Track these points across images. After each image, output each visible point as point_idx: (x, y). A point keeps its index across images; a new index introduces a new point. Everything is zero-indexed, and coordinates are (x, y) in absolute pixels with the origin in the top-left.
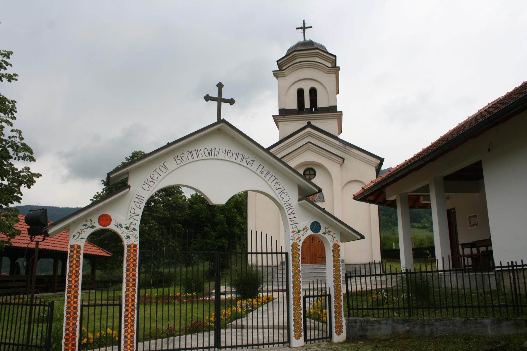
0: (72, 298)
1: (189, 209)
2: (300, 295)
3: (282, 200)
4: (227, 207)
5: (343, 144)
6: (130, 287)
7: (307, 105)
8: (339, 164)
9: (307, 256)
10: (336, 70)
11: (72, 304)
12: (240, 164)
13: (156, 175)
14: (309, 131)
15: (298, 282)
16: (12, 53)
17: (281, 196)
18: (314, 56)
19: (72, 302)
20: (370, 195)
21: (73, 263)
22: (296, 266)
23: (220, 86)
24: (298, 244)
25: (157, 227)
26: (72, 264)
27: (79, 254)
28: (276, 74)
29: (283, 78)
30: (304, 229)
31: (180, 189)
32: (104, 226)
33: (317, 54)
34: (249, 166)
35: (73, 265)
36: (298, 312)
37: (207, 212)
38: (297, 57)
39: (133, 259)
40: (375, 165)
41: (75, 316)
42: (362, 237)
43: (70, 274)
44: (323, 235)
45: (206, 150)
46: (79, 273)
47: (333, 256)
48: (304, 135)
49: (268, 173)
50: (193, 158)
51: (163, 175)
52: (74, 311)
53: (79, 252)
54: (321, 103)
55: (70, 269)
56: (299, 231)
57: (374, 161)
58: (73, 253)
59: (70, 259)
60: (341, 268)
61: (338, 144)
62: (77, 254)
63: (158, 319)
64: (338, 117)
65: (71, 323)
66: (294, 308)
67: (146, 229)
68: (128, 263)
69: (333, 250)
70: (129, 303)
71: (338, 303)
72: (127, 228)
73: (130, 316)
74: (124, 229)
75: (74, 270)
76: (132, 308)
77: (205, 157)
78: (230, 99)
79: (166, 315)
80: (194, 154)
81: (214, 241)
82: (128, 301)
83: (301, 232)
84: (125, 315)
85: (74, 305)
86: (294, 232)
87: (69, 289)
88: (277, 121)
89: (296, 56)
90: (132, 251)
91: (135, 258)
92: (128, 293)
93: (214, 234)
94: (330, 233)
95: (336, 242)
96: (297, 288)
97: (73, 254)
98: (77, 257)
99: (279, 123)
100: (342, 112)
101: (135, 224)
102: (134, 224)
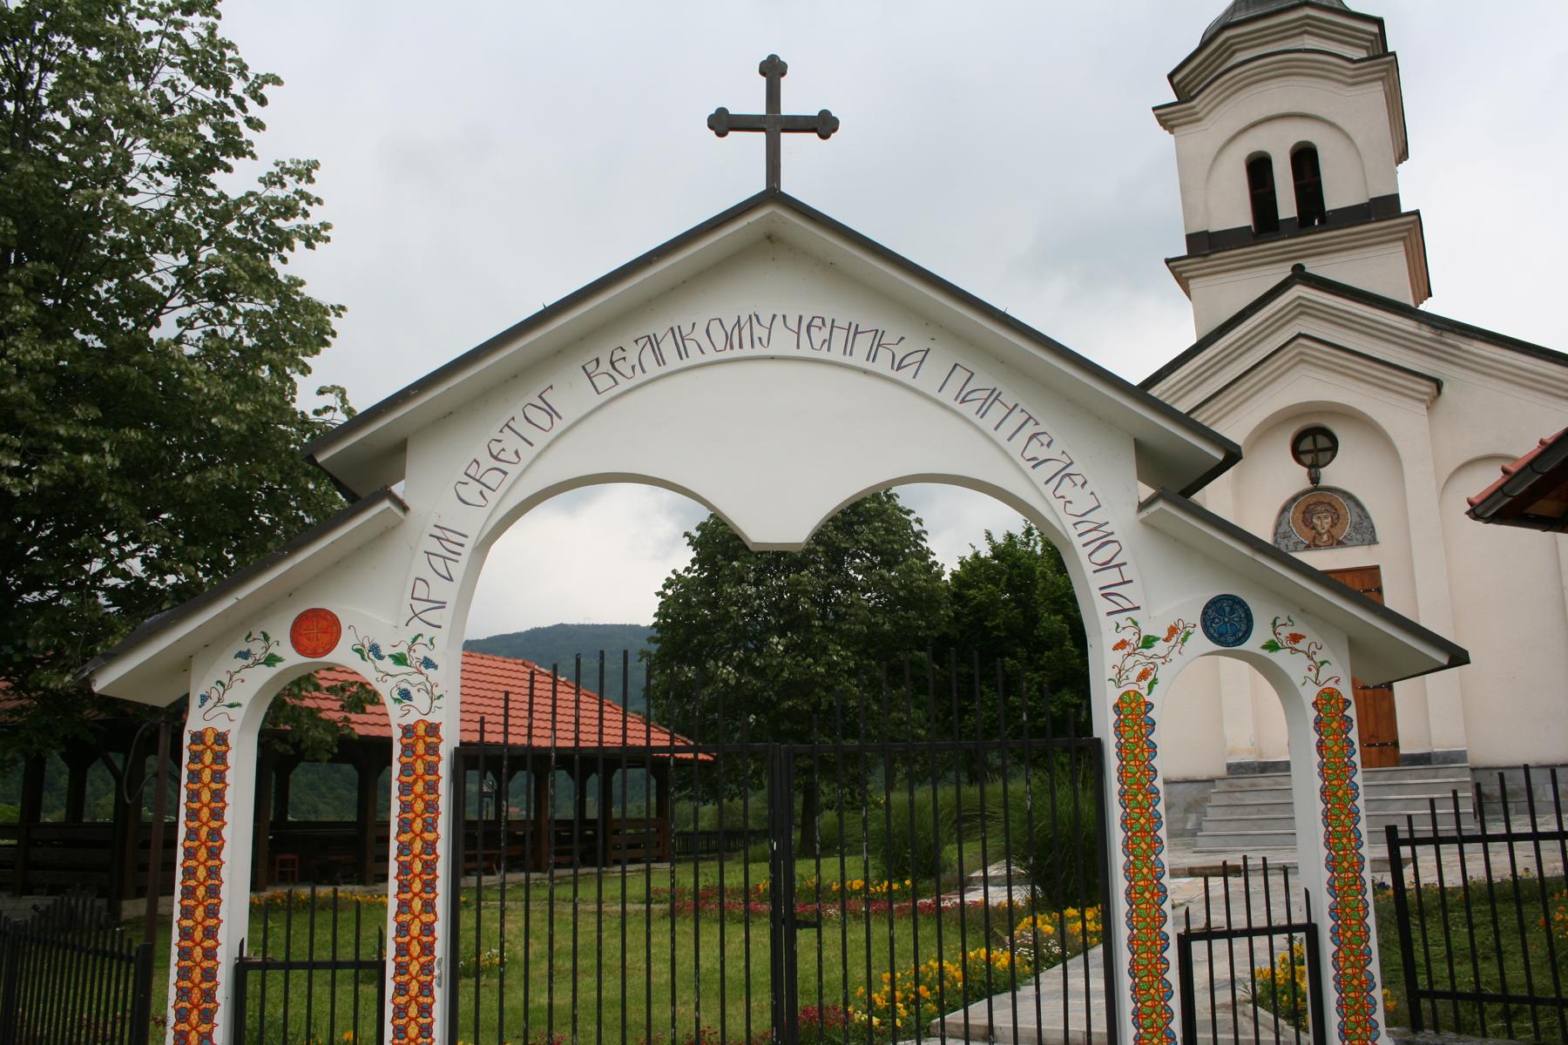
0: (198, 935)
1: (952, 604)
2: (1164, 929)
3: (1061, 514)
5: (1434, 327)
6: (416, 895)
7: (1287, 207)
8: (1423, 401)
11: (198, 960)
12: (865, 372)
13: (511, 442)
14: (1299, 297)
15: (1150, 870)
16: (316, 165)
17: (1058, 493)
19: (198, 952)
20: (1534, 493)
21: (200, 800)
22: (1140, 797)
23: (773, 70)
24: (1148, 699)
25: (852, 664)
26: (196, 805)
27: (223, 768)
28: (1166, 117)
29: (1194, 125)
30: (1173, 631)
31: (923, 543)
32: (314, 654)
33: (1309, 25)
34: (905, 375)
35: (199, 810)
36: (1154, 1007)
37: (1012, 610)
38: (1234, 48)
39: (426, 783)
41: (207, 1005)
42: (1458, 657)
43: (188, 844)
44: (1265, 653)
45: (715, 326)
46: (221, 839)
47: (1321, 747)
49: (994, 396)
50: (660, 360)
51: (540, 439)
52: (204, 986)
53: (433, 749)
54: (1338, 194)
55: (191, 824)
56: (1148, 642)
58: (201, 761)
59: (191, 786)
60: (1360, 803)
61: (1417, 331)
62: (215, 767)
63: (580, 1013)
64: (1406, 234)
65: (194, 1033)
66: (1135, 989)
67: (817, 673)
68: (404, 798)
69: (1318, 723)
70: (412, 959)
71: (1353, 966)
72: (399, 659)
73: (413, 1011)
74: (388, 665)
75: (205, 830)
76: (422, 978)
77: (711, 356)
78: (816, 114)
79: (735, 970)
80: (668, 348)
81: (1035, 702)
82: (408, 950)
83: (1157, 644)
84: (397, 1006)
85: (205, 964)
86: (1122, 645)
87: (185, 902)
88: (1184, 275)
89: (1232, 45)
90: (420, 749)
91: (433, 778)
92: (408, 917)
93: (1037, 677)
94: (1297, 646)
95: (1331, 684)
96: (1147, 895)
97: (199, 766)
98: (213, 780)
99: (1191, 282)
100: (1417, 213)
101: (431, 641)
102: (428, 642)
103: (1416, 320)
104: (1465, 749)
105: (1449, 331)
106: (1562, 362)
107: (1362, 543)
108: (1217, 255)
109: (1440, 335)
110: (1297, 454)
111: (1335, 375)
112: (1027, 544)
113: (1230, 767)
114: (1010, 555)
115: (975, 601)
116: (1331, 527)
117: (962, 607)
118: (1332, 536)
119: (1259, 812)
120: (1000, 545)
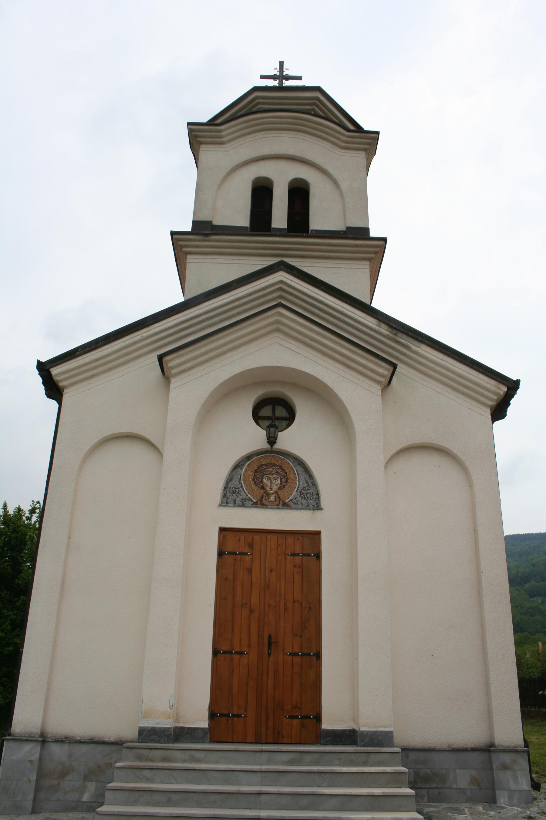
5: (391, 327)
8: (378, 382)
9: (246, 710)
10: (370, 141)
14: (281, 282)
33: (317, 106)
40: (491, 400)
48: (266, 292)
57: (488, 386)
64: (378, 249)
88: (184, 249)
99: (188, 256)
104: (391, 729)
106: (490, 375)
108: (217, 237)
109: (396, 334)
110: (257, 417)
116: (279, 488)
118: (279, 498)
119: (169, 803)
120: (10, 515)
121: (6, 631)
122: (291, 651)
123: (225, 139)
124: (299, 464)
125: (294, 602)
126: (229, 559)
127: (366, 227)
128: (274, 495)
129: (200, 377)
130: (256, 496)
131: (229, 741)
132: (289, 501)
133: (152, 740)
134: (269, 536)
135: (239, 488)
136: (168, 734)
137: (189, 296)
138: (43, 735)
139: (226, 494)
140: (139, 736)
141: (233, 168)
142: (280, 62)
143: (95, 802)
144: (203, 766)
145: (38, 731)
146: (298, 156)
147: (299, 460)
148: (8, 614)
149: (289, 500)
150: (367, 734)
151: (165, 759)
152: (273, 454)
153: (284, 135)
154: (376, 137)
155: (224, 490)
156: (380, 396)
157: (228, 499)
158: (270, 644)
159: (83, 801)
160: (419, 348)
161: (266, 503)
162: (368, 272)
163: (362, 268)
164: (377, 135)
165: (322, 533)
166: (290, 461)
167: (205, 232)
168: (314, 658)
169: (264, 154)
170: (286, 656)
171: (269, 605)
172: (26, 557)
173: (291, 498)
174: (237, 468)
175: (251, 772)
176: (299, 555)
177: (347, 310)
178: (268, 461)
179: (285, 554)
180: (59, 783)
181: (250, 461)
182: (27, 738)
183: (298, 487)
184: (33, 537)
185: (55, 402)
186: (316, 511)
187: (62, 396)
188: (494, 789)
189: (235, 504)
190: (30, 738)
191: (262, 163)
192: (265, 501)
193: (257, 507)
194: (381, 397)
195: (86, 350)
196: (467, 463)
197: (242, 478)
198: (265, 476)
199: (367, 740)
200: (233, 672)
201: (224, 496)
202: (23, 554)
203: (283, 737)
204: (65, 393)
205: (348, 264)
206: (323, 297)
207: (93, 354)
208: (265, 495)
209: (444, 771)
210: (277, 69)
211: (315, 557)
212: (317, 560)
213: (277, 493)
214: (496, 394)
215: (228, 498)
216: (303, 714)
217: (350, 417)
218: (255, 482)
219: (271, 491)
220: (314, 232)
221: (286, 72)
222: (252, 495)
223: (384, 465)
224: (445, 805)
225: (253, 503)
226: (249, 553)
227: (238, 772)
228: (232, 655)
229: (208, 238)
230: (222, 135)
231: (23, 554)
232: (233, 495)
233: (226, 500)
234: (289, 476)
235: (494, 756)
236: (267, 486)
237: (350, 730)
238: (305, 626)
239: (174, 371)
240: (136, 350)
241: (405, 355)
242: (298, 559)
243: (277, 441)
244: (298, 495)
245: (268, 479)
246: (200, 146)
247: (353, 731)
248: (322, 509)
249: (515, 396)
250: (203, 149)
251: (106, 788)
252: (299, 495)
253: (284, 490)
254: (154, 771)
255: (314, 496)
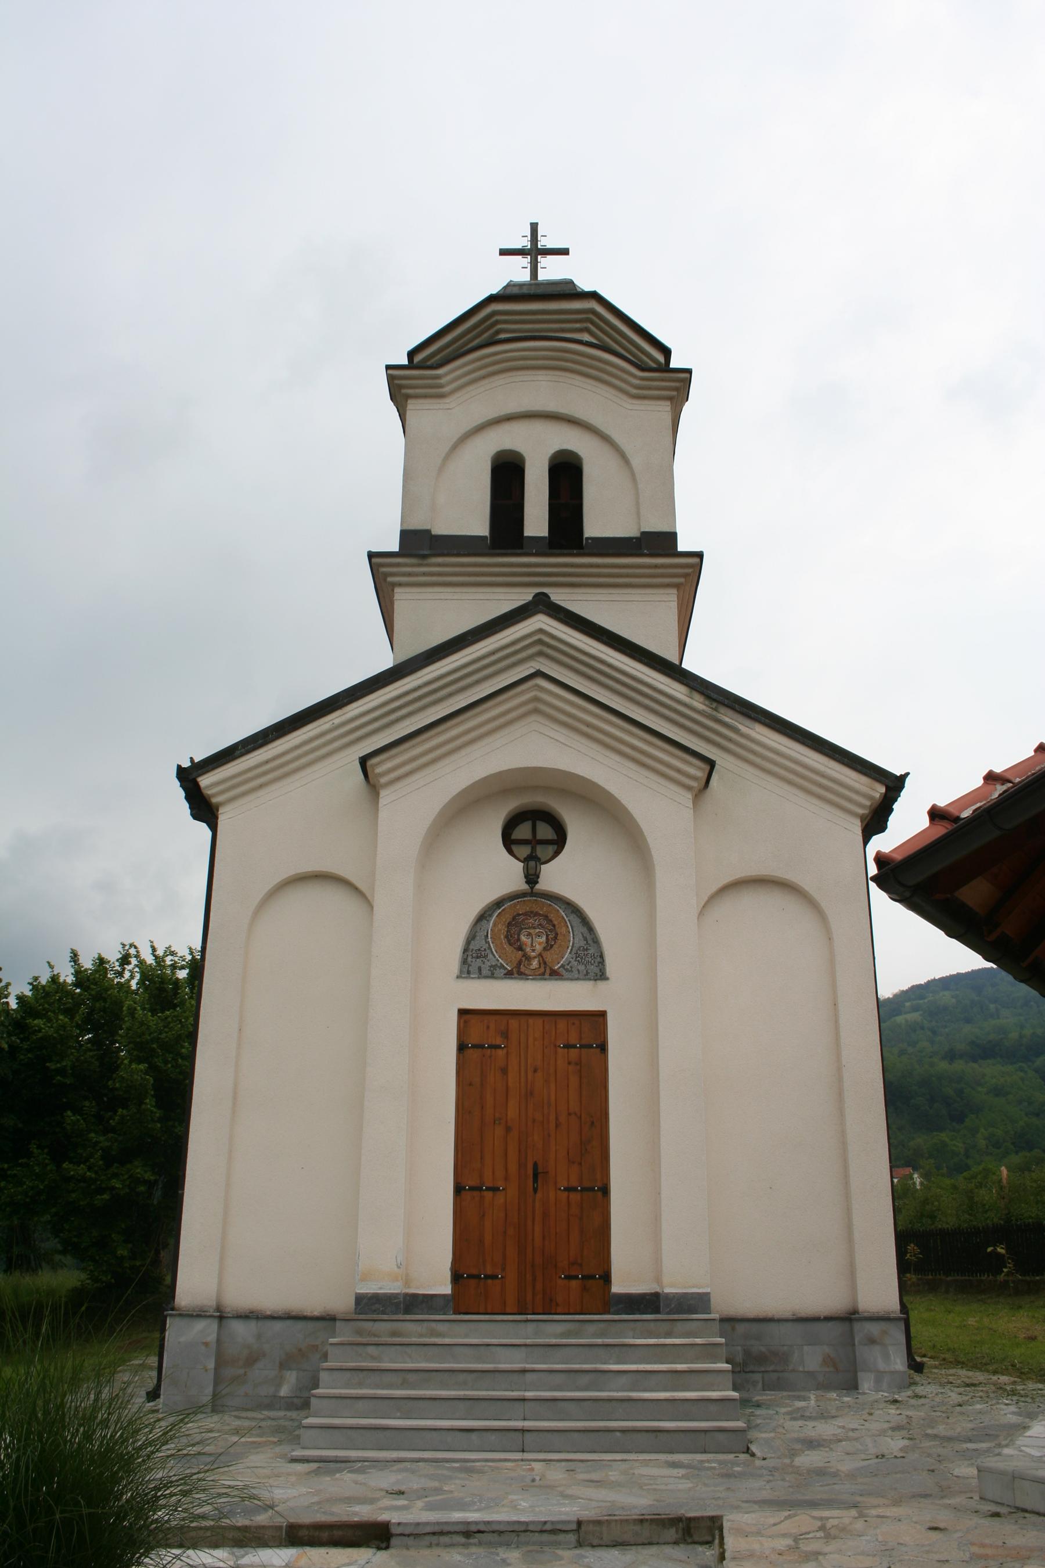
1: (10, 1034)
4: (163, 1036)
5: (708, 697)
8: (688, 788)
9: (504, 1269)
10: (677, 384)
14: (541, 631)
18: (578, 325)
38: (499, 326)
57: (857, 786)
64: (681, 580)
81: (96, 1173)
88: (389, 579)
89: (497, 322)
103: (686, 685)
104: (708, 1290)
105: (727, 706)
106: (859, 767)
107: (586, 977)
108: (440, 560)
109: (715, 709)
110: (509, 842)
111: (577, 737)
112: (120, 974)
113: (360, 1299)
114: (96, 984)
115: (40, 1035)
116: (545, 949)
117: (22, 1040)
118: (545, 963)
119: (404, 1385)
120: (86, 970)
121: (96, 1168)
122: (566, 1185)
123: (447, 389)
124: (573, 912)
125: (569, 1114)
126: (473, 1055)
127: (672, 531)
128: (537, 960)
129: (422, 786)
130: (511, 961)
131: (481, 1311)
132: (559, 968)
133: (375, 1311)
134: (531, 1021)
135: (485, 950)
136: (396, 1302)
137: (403, 657)
138: (218, 1309)
139: (467, 959)
140: (356, 1305)
141: (461, 437)
142: (532, 224)
143: (297, 1397)
144: (447, 1341)
145: (214, 1303)
146: (562, 414)
147: (573, 906)
148: (97, 1140)
149: (559, 965)
150: (674, 1296)
151: (394, 1334)
152: (535, 898)
153: (540, 378)
154: (687, 378)
155: (464, 953)
156: (691, 809)
157: (470, 967)
158: (536, 1176)
159: (280, 1397)
160: (752, 729)
161: (526, 972)
162: (674, 605)
163: (666, 600)
164: (687, 375)
165: (608, 1015)
166: (560, 908)
167: (422, 552)
168: (600, 1194)
169: (509, 412)
170: (559, 1192)
171: (534, 1121)
172: (125, 1044)
173: (562, 962)
174: (482, 920)
175: (512, 1347)
176: (574, 1046)
177: (642, 672)
178: (528, 908)
179: (555, 1046)
180: (245, 1372)
181: (501, 909)
182: (199, 1313)
183: (573, 947)
184: (135, 1009)
185: (204, 825)
186: (599, 983)
187: (217, 818)
188: (855, 1372)
189: (480, 974)
190: (203, 1313)
191: (507, 427)
192: (524, 968)
193: (512, 978)
194: (692, 810)
195: (249, 747)
196: (824, 904)
197: (489, 935)
198: (524, 931)
199: (673, 1306)
200: (484, 1215)
201: (464, 962)
202: (119, 1038)
203: (557, 1305)
204: (220, 814)
205: (644, 594)
206: (605, 653)
207: (261, 754)
208: (523, 959)
209: (785, 1348)
210: (526, 236)
211: (599, 1049)
212: (601, 1053)
213: (542, 957)
214: (870, 798)
215: (469, 965)
216: (585, 1273)
217: (647, 841)
218: (509, 941)
219: (532, 954)
220: (590, 541)
221: (543, 243)
222: (505, 960)
223: (697, 915)
224: (785, 1393)
225: (507, 973)
226: (503, 1046)
227: (494, 1347)
228: (482, 1192)
229: (425, 562)
230: (441, 383)
231: (119, 1038)
232: (478, 960)
233: (467, 968)
234: (559, 931)
235: (857, 1326)
236: (526, 945)
237: (652, 1294)
238: (586, 1150)
239: (383, 780)
240: (325, 745)
241: (730, 740)
242: (573, 1053)
243: (539, 880)
244: (572, 958)
245: (527, 936)
246: (407, 401)
247: (656, 1295)
248: (607, 979)
249: (899, 799)
250: (412, 405)
251: (321, 1368)
252: (574, 959)
253: (552, 951)
254: (381, 1348)
255: (596, 958)
